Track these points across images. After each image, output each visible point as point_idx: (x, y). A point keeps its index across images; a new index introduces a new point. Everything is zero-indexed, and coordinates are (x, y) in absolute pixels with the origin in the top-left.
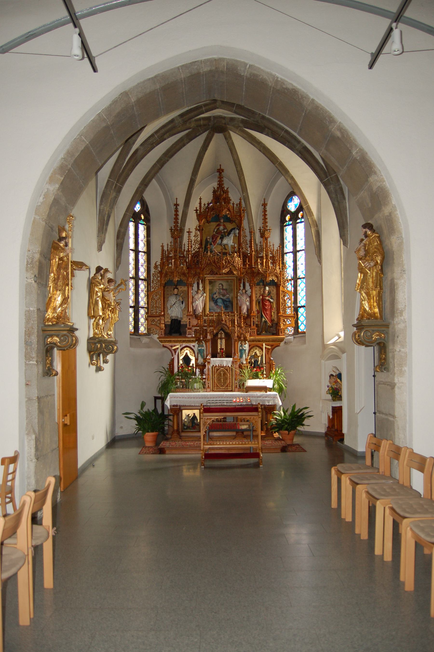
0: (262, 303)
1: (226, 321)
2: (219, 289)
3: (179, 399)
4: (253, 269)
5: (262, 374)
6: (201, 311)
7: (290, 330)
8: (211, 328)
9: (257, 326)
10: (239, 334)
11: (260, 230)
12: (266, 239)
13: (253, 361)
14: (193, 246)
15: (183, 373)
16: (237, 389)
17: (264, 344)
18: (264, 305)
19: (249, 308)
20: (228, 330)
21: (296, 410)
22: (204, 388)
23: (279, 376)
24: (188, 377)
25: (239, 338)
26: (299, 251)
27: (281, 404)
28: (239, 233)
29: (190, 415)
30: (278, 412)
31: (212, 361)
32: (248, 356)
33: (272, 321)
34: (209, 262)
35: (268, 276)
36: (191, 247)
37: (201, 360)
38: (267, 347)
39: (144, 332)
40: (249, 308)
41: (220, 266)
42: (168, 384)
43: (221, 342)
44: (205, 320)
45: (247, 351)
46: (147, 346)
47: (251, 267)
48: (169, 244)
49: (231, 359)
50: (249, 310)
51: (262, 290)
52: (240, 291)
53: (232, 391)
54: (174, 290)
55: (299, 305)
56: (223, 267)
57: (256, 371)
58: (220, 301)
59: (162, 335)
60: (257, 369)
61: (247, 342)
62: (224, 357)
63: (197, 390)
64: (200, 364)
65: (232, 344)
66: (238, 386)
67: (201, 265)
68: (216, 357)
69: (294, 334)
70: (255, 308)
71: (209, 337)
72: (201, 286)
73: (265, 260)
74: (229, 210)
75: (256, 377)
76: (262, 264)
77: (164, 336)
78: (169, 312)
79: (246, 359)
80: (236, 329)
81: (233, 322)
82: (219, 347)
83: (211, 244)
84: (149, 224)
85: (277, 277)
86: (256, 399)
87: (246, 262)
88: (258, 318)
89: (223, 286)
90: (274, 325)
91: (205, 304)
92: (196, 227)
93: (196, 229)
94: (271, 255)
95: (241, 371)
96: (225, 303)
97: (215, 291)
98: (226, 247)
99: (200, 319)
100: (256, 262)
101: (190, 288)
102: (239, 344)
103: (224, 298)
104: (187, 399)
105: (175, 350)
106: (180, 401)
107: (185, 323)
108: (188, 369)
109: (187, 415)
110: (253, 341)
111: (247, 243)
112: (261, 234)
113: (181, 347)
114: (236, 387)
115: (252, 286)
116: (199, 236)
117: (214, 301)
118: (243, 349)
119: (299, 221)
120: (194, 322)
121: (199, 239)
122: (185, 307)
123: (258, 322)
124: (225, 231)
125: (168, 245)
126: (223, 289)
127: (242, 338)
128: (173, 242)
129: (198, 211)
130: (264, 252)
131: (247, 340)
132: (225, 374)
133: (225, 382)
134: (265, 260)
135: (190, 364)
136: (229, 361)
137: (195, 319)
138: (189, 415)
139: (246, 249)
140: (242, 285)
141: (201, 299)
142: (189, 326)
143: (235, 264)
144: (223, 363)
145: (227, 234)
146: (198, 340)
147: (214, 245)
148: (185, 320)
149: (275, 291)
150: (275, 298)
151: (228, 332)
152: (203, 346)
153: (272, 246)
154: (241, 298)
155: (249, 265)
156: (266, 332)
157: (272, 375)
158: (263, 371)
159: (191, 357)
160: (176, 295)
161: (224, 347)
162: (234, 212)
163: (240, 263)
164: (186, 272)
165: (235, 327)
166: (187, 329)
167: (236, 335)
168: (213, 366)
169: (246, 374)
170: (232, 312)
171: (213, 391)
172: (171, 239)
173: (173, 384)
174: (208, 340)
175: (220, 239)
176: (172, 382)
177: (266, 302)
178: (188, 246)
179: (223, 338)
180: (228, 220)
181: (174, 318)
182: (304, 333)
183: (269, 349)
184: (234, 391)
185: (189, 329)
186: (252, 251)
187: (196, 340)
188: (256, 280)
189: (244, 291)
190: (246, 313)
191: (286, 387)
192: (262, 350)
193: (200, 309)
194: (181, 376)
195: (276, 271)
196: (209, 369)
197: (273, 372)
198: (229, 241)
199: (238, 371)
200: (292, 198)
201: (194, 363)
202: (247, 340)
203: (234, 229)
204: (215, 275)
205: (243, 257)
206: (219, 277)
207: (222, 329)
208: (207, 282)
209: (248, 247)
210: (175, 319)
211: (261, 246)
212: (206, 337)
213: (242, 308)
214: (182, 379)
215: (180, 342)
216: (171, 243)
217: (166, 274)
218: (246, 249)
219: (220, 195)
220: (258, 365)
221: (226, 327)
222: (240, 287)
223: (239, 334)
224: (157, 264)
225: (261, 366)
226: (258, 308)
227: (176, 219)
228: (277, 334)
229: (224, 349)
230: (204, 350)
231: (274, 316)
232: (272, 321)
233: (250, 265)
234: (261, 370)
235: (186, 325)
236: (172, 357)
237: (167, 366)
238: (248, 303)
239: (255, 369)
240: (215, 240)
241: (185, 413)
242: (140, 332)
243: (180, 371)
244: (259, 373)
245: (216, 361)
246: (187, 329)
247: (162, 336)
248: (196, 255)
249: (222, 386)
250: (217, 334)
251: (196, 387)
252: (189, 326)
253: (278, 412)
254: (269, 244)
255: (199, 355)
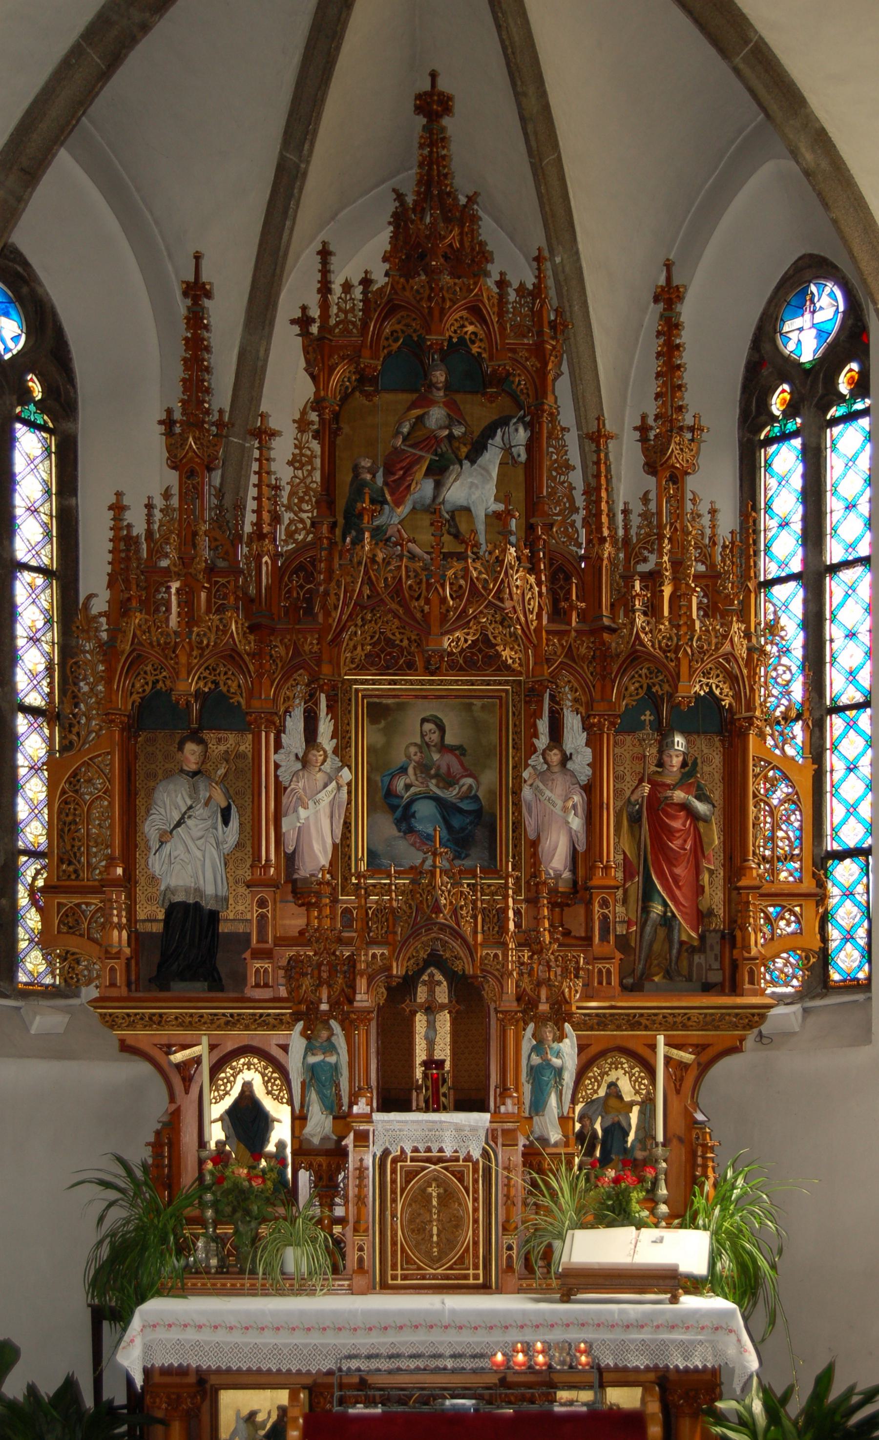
0: (652, 817)
1: (455, 912)
2: (424, 746)
3: (191, 1335)
4: (606, 636)
5: (651, 1200)
6: (324, 860)
7: (782, 977)
8: (378, 952)
9: (623, 943)
10: (526, 984)
11: (643, 429)
12: (677, 477)
13: (598, 1127)
14: (287, 516)
15: (227, 1193)
16: (512, 1280)
17: (661, 1039)
18: (660, 833)
19: (581, 848)
20: (467, 960)
21: (836, 1392)
22: (335, 1270)
23: (737, 1210)
24: (248, 1212)
25: (527, 1003)
26: (835, 569)
27: (754, 1364)
28: (532, 446)
29: (260, 1418)
30: (733, 1404)
31: (380, 1127)
32: (574, 1101)
33: (701, 917)
34: (367, 592)
35: (684, 669)
36: (276, 519)
37: (320, 1124)
38: (677, 1054)
39: (48, 980)
40: (581, 848)
41: (426, 616)
42: (144, 1248)
43: (431, 1025)
44: (347, 911)
45: (569, 1078)
46: (55, 1049)
47: (594, 628)
48: (159, 502)
49: (481, 1119)
50: (584, 859)
51: (651, 752)
52: (536, 760)
53: (485, 1288)
54: (181, 748)
55: (831, 845)
56: (444, 618)
57: (617, 1180)
58: (425, 810)
59: (113, 985)
60: (622, 1173)
61: (567, 1026)
62: (445, 1109)
63: (300, 1286)
64: (316, 1141)
65: (487, 1041)
66: (518, 1265)
67: (328, 614)
68: (404, 1106)
69: (800, 996)
70: (615, 847)
71: (363, 999)
72: (325, 727)
73: (667, 590)
74: (476, 312)
75: (614, 1213)
76: (653, 610)
77: (124, 991)
78: (156, 864)
79: (564, 1120)
80: (512, 956)
81: (496, 919)
82: (420, 1055)
83: (379, 501)
84: (67, 426)
85: (732, 679)
86: (618, 1335)
87: (568, 598)
88: (625, 902)
89: (441, 728)
90: (713, 940)
91: (347, 825)
92: (303, 413)
93: (302, 424)
94: (702, 568)
95: (534, 1184)
96: (456, 822)
97: (400, 759)
98: (463, 527)
99: (317, 905)
100: (623, 602)
101: (267, 739)
102: (528, 1042)
103: (451, 794)
104: (237, 1338)
105: (186, 1070)
106: (198, 1343)
107: (241, 928)
108: (252, 1168)
109: (245, 1412)
110: (601, 1021)
111: (572, 500)
112: (645, 451)
113: (218, 1054)
114: (510, 1268)
115: (600, 726)
116: (318, 462)
117: (393, 808)
118: (548, 1064)
119: (836, 411)
120: (293, 920)
121: (317, 476)
122: (239, 845)
123: (629, 923)
124: (458, 431)
125: (149, 506)
126: (443, 748)
127: (544, 1007)
128: (175, 490)
129: (314, 329)
130: (667, 547)
131: (569, 1017)
132: (448, 1197)
133: (448, 1242)
134: (667, 590)
135: (265, 1140)
136: (474, 1129)
137: (292, 908)
138: (252, 1415)
139: (566, 533)
140: (543, 726)
141: (325, 797)
142: (262, 939)
143: (508, 604)
144: (440, 1139)
145: (464, 450)
146: (310, 1018)
147: (398, 503)
148: (240, 913)
149: (717, 760)
150: (717, 795)
151: (470, 971)
152: (331, 1048)
153: (706, 521)
154: (538, 792)
155: (583, 616)
156: (668, 975)
157: (699, 1202)
158: (655, 1183)
159: (269, 1104)
160: (195, 774)
161: (443, 1051)
162: (502, 328)
163: (534, 605)
164: (243, 647)
165: (505, 945)
166: (247, 955)
167: (510, 987)
168: (386, 1153)
169: (566, 1198)
170: (492, 869)
171: (385, 1287)
172: (172, 478)
173: (169, 1250)
174: (364, 1015)
175: (428, 474)
176: (164, 1240)
177: (674, 818)
178: (258, 512)
179: (442, 1007)
180: (474, 376)
181: (179, 898)
182: (852, 986)
183: (683, 1067)
184: (499, 1290)
185: (259, 954)
186: (603, 540)
187: (297, 1017)
188: (624, 692)
189: (555, 757)
190: (567, 875)
191: (773, 1267)
192: (651, 1072)
193: (318, 854)
194: (215, 1205)
195: (727, 647)
196: (361, 1170)
197: (708, 1187)
198: (475, 489)
199: (518, 1180)
200: (805, 291)
201: (288, 1138)
202: (569, 1017)
203: (503, 422)
204: (400, 671)
205: (553, 579)
206: (421, 682)
207: (435, 960)
208: (358, 712)
209: (579, 524)
210: (184, 905)
211: (644, 515)
212: (351, 1001)
213: (546, 845)
214: (216, 1223)
215: (213, 1022)
216: (167, 495)
217: (136, 660)
218: (570, 538)
219: (433, 225)
220: (625, 1150)
221: (456, 945)
222: (536, 735)
223: (526, 984)
224: (94, 611)
225: (639, 1155)
226: (626, 844)
227: (196, 350)
228: (735, 989)
229: (447, 1066)
230: (336, 1067)
231: (715, 897)
232: (701, 917)
233: (591, 616)
234: (641, 1180)
235: (248, 936)
236: (173, 1107)
237: (139, 1154)
238: (576, 823)
239: (611, 1173)
240: (403, 477)
241: (233, 1403)
242: (22, 978)
243: (208, 1178)
244: (634, 1195)
245: (402, 1130)
246: (247, 955)
247: (114, 992)
248: (300, 567)
249: (435, 1261)
250: (408, 984)
251: (290, 1267)
252: (262, 939)
253: (733, 1404)
254: (689, 506)
255: (313, 1096)
